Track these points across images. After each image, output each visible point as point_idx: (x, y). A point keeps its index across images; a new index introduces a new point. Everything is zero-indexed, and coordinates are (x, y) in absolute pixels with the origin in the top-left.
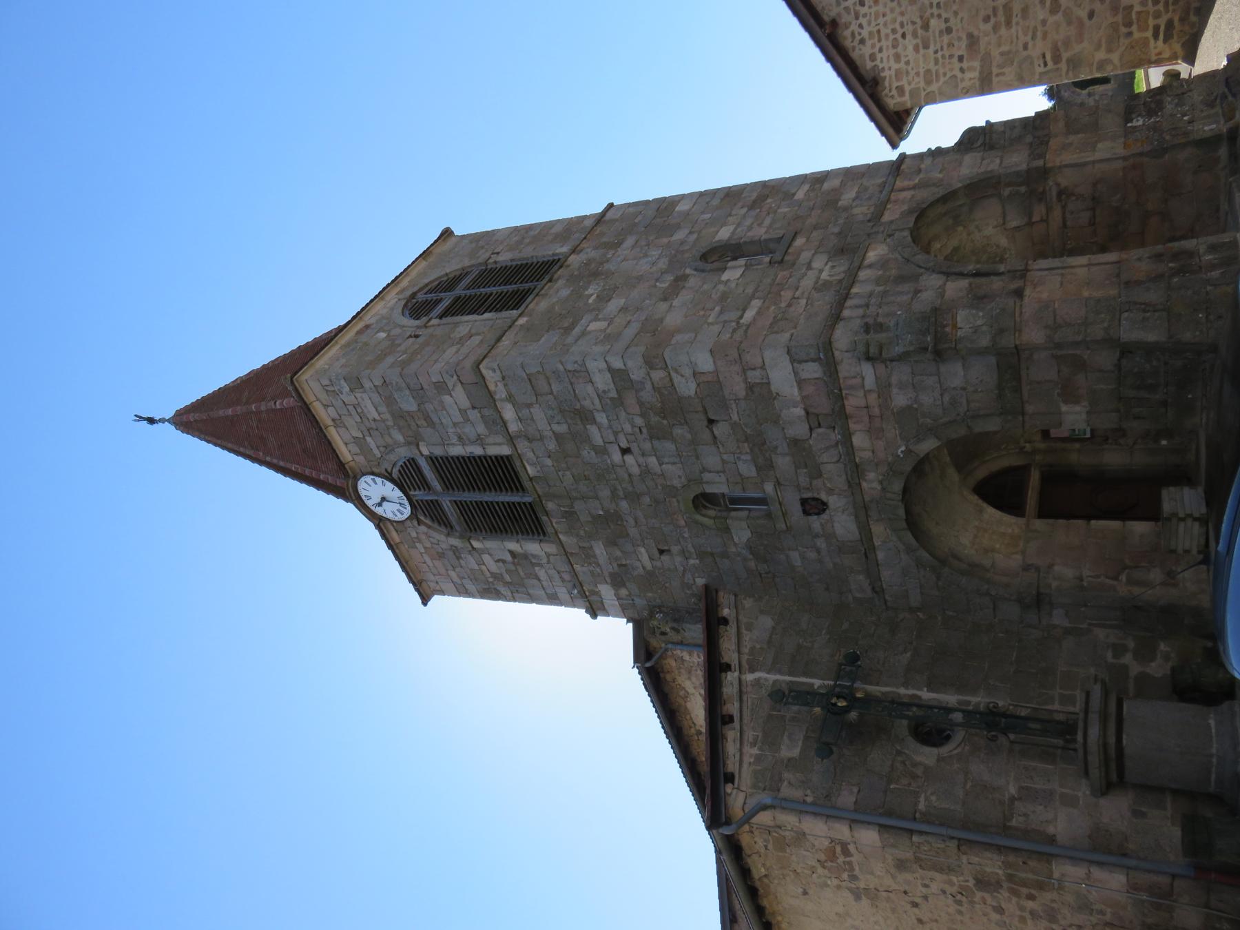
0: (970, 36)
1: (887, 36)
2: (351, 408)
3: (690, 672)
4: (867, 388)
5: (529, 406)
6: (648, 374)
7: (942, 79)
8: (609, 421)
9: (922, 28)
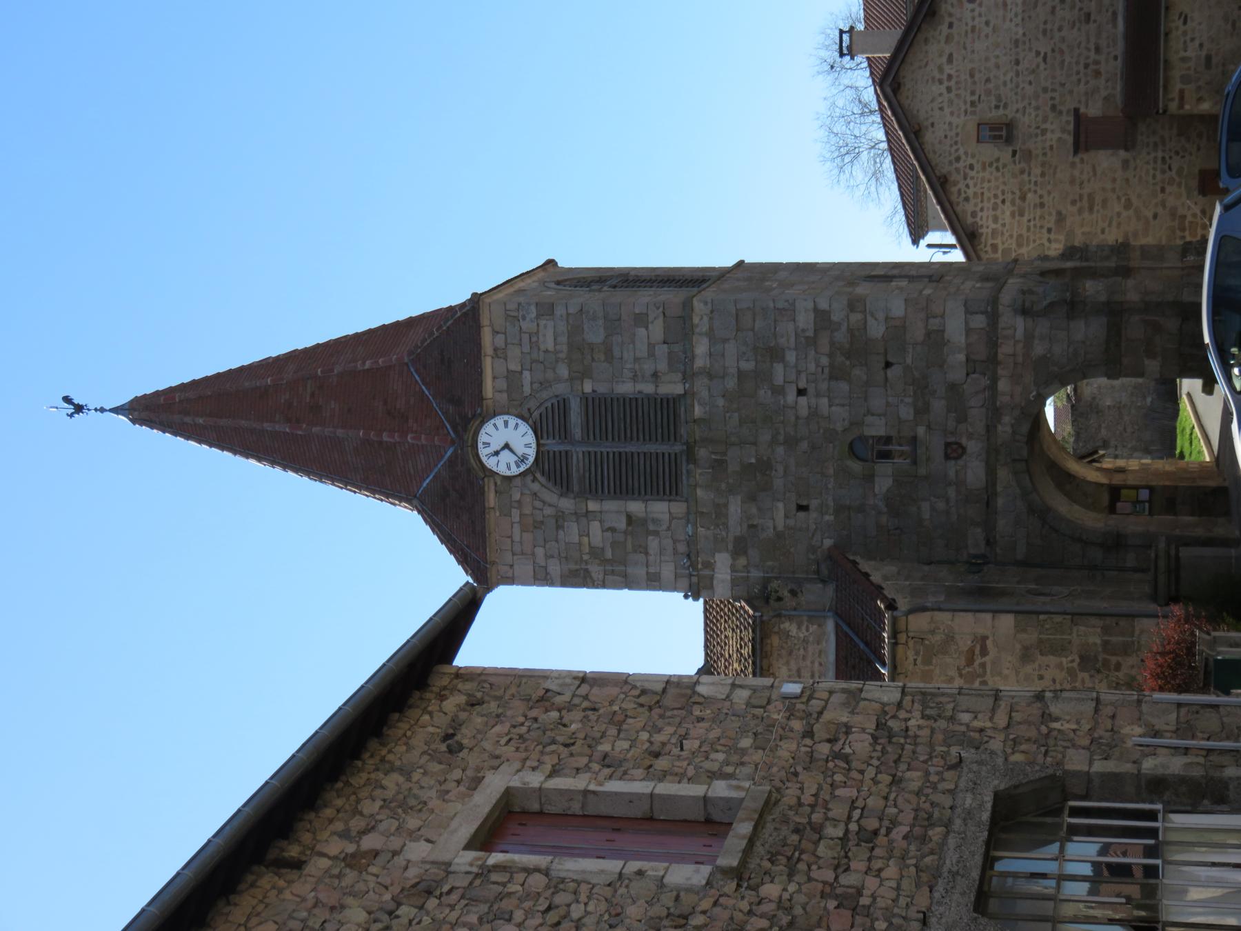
0: (1059, 213)
1: (989, 199)
2: (526, 338)
3: (790, 653)
4: (1017, 338)
5: (725, 341)
6: (848, 317)
7: (1032, 245)
8: (797, 359)
9: (1020, 198)
